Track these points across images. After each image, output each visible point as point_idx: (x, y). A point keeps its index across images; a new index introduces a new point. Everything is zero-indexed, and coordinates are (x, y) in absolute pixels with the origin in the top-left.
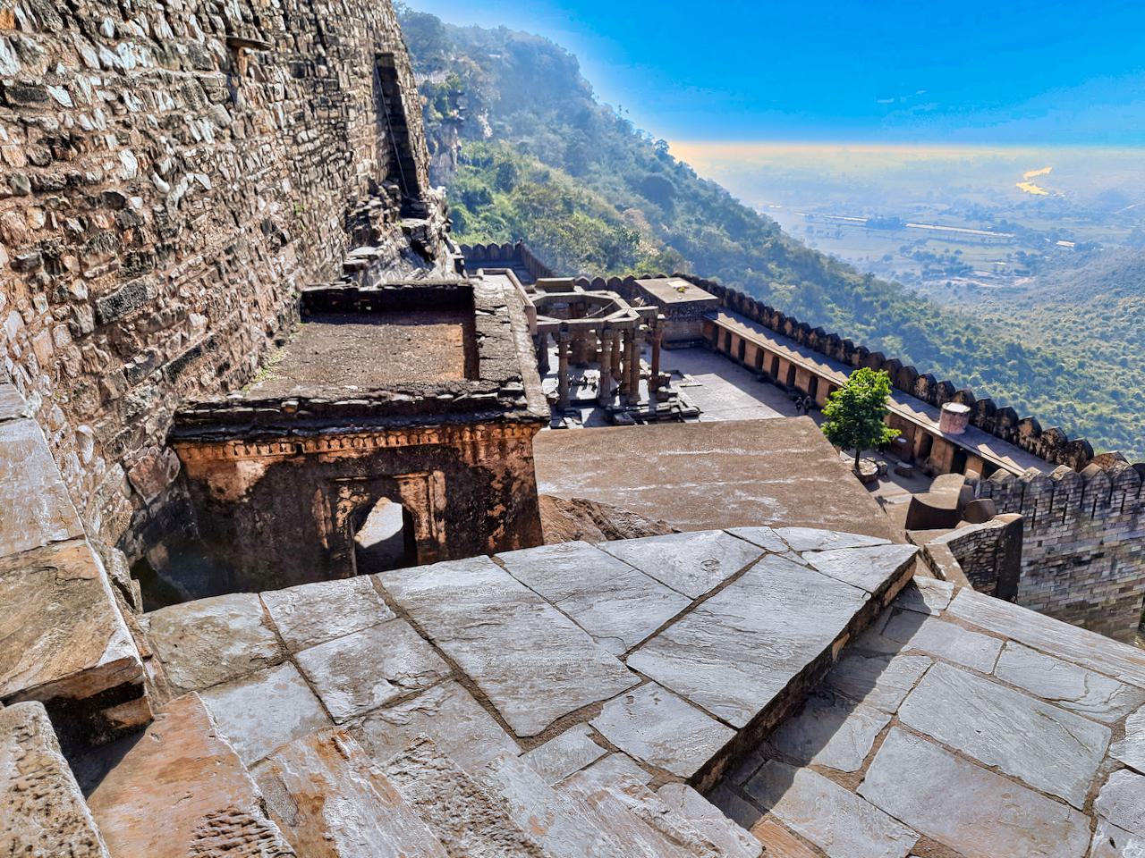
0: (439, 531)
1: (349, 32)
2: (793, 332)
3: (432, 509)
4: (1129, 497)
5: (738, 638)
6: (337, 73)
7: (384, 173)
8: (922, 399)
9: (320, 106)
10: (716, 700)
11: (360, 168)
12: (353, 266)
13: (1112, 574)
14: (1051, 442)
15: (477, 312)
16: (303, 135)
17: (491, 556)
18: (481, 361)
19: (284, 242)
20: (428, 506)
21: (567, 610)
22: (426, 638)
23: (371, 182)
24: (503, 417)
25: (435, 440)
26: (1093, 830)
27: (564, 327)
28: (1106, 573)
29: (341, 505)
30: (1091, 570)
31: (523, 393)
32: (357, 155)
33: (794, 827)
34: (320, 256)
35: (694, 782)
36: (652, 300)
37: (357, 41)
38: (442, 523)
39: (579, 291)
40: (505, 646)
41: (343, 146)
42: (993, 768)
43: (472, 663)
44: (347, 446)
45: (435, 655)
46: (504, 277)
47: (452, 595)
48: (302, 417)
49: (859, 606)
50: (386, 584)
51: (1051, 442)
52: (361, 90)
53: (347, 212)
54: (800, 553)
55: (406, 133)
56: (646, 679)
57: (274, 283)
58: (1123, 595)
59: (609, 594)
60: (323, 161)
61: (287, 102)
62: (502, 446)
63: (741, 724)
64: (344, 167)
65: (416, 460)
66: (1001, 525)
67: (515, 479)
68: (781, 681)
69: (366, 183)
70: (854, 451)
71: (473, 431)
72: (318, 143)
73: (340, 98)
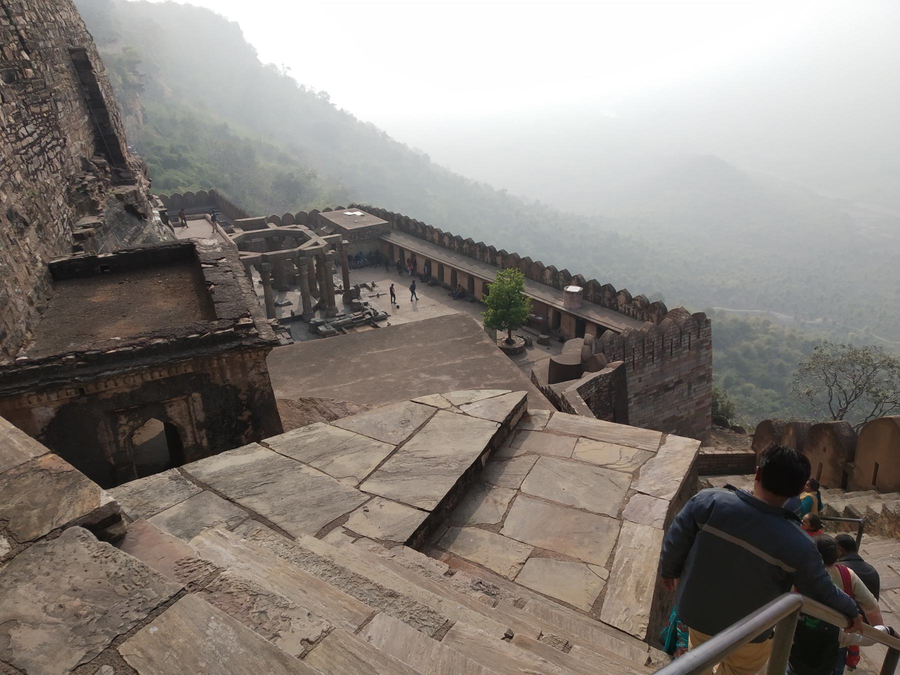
0: (202, 438)
1: (46, 35)
2: (450, 244)
3: (194, 422)
4: (693, 338)
5: (426, 462)
6: (42, 73)
7: (91, 150)
8: (550, 285)
9: (32, 104)
10: (417, 498)
11: (73, 150)
12: (81, 234)
13: (689, 394)
14: (639, 305)
15: (203, 265)
16: (23, 130)
17: (259, 442)
18: (216, 305)
19: (26, 224)
20: (191, 420)
21: (317, 466)
22: (228, 499)
23: (83, 160)
24: (241, 345)
25: (190, 370)
26: (621, 526)
27: (265, 258)
28: (685, 394)
29: (121, 430)
30: (675, 393)
31: (253, 325)
32: (69, 140)
33: (466, 558)
34: (54, 232)
35: (408, 543)
36: (337, 229)
37: (53, 42)
38: (204, 432)
39: (272, 227)
40: (280, 494)
41: (56, 134)
42: (571, 507)
43: (261, 506)
44: (121, 384)
45: (236, 508)
46: (204, 221)
47: (237, 471)
48: (79, 367)
49: (494, 432)
50: (190, 472)
51: (639, 305)
52: (64, 83)
53: (68, 190)
54: (458, 407)
55: (107, 114)
56: (373, 496)
57: (26, 261)
58: (699, 407)
59: (343, 452)
60: (42, 151)
61: (5, 105)
62: (243, 366)
63: (431, 508)
64: (60, 153)
65: (177, 387)
66: (611, 370)
67: (257, 389)
68: (453, 481)
69: (80, 162)
70: (507, 330)
71: (219, 359)
72: (35, 136)
73: (48, 94)
